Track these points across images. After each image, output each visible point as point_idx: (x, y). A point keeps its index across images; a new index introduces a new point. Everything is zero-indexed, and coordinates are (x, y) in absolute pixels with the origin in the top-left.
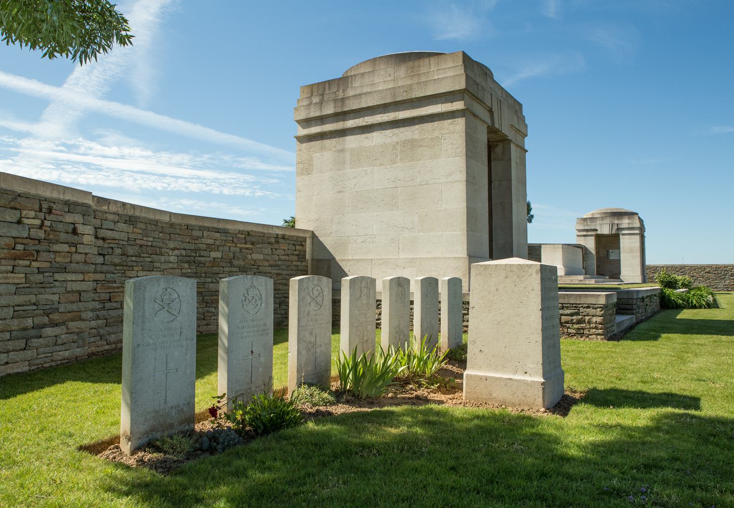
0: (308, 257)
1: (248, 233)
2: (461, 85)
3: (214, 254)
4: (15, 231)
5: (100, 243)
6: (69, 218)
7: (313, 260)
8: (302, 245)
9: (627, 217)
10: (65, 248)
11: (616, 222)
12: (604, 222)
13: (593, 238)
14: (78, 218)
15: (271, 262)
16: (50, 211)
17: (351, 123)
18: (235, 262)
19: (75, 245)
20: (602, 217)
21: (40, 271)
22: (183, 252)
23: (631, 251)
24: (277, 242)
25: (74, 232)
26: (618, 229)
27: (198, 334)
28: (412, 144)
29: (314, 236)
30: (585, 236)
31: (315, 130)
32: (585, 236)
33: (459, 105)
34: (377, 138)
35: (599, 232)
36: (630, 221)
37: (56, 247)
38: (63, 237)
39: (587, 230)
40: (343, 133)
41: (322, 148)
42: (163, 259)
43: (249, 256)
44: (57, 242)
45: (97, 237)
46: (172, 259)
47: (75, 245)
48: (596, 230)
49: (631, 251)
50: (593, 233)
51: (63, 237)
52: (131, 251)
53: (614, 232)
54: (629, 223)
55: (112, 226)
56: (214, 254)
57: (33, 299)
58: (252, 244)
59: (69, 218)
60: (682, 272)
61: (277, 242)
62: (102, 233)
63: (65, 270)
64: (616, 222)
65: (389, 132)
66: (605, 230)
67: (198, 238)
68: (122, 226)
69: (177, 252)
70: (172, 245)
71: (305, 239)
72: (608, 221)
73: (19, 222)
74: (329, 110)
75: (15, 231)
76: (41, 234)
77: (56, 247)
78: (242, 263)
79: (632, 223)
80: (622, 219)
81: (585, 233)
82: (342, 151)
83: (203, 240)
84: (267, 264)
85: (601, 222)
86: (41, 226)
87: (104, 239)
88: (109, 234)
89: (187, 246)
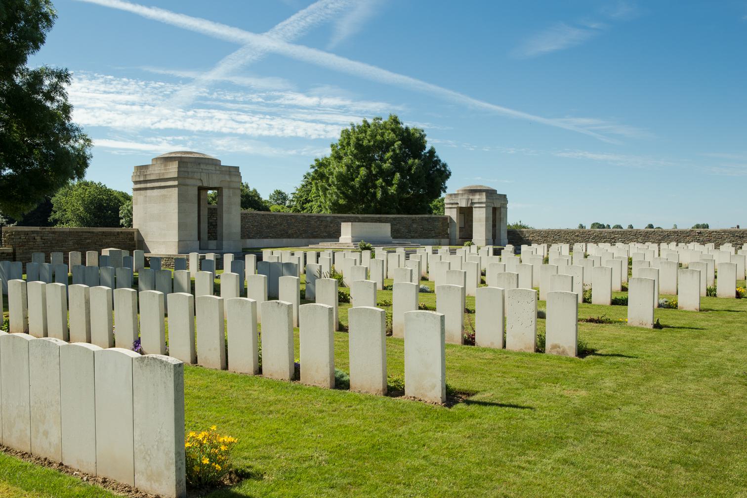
0: (135, 239)
1: (103, 232)
2: (176, 176)
3: (88, 241)
4: (19, 240)
5: (43, 241)
6: (32, 235)
7: (138, 240)
8: (132, 235)
9: (478, 193)
10: (32, 243)
11: (471, 197)
12: (463, 197)
13: (456, 210)
14: (35, 235)
15: (115, 243)
16: (27, 234)
17: (149, 185)
18: (97, 243)
19: (35, 242)
20: (462, 194)
21: (26, 249)
22: (75, 241)
23: (480, 220)
24: (118, 235)
25: (34, 239)
26: (472, 203)
27: (216, 294)
28: (164, 196)
29: (138, 231)
30: (450, 208)
31: (142, 186)
32: (450, 208)
33: (176, 183)
34: (156, 192)
35: (460, 206)
36: (480, 197)
37: (30, 243)
38: (31, 240)
39: (452, 204)
40: (146, 189)
41: (140, 195)
42: (66, 243)
43: (104, 241)
44: (30, 242)
45: (42, 239)
46: (70, 243)
47: (35, 242)
48: (457, 204)
49: (480, 220)
50: (456, 206)
51: (31, 240)
52: (53, 242)
53: (469, 206)
54: (479, 199)
55: (47, 235)
56: (88, 241)
57: (24, 256)
58: (105, 236)
59: (32, 235)
60: (559, 236)
61: (118, 235)
62: (43, 238)
63: (32, 249)
64: (471, 197)
65: (159, 190)
66: (463, 204)
67: (81, 235)
68: (50, 235)
69: (72, 241)
70: (70, 238)
71: (133, 233)
72: (466, 197)
73: (20, 238)
74: (142, 179)
75: (19, 240)
76: (25, 240)
77: (30, 243)
78: (100, 243)
79: (481, 199)
80: (474, 195)
81: (450, 206)
82: (146, 196)
83: (84, 236)
84: (112, 243)
85: (461, 197)
86: (26, 238)
87: (44, 239)
88: (46, 238)
89: (77, 239)
